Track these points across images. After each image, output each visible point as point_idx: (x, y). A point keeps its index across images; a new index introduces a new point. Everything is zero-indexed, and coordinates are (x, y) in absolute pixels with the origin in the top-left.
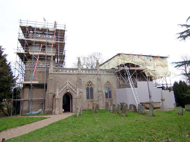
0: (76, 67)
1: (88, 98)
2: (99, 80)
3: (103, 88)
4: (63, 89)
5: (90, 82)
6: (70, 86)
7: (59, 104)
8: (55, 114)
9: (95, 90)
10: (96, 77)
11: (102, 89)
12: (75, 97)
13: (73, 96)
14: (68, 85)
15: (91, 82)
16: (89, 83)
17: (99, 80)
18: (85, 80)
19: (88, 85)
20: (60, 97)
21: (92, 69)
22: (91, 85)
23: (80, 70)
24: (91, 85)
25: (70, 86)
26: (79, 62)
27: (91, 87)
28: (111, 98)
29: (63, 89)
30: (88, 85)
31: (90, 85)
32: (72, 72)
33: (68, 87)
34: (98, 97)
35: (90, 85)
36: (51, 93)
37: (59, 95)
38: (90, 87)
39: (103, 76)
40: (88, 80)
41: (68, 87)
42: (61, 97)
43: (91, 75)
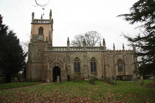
0: (66, 46)
1: (92, 71)
2: (85, 56)
3: (88, 63)
4: (53, 63)
5: (77, 58)
6: (58, 61)
7: (50, 76)
8: (26, 81)
9: (82, 65)
10: (83, 54)
11: (87, 64)
12: (62, 70)
13: (60, 69)
14: (57, 60)
15: (78, 58)
16: (93, 59)
17: (85, 56)
18: (73, 56)
19: (92, 60)
20: (51, 70)
21: (80, 47)
22: (94, 60)
23: (68, 48)
24: (94, 60)
25: (58, 61)
26: (68, 42)
27: (95, 62)
28: (79, 72)
29: (53, 63)
30: (92, 60)
31: (77, 60)
32: (76, 50)
33: (57, 62)
34: (84, 70)
35: (77, 60)
36: (46, 66)
37: (50, 69)
38: (93, 62)
39: (89, 53)
40: (76, 57)
41: (57, 62)
42: (51, 70)
43: (78, 52)
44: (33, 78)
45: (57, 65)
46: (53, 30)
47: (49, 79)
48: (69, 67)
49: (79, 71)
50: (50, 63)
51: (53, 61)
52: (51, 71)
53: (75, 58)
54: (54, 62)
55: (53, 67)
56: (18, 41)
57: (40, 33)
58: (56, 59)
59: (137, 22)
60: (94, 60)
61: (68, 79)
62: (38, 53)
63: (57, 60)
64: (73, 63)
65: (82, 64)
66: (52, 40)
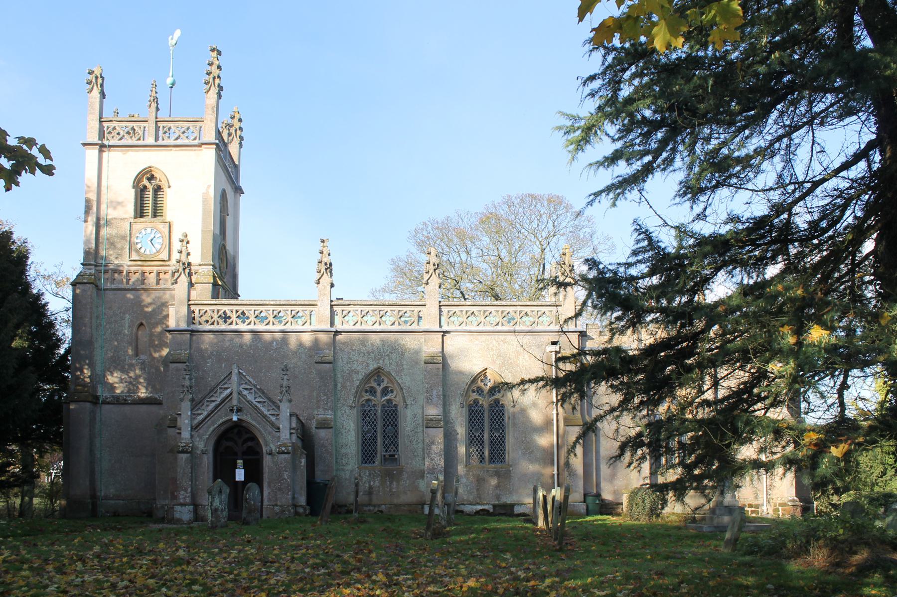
4: (213, 404)
6: (245, 392)
9: (408, 420)
24: (385, 391)
25: (245, 392)
27: (389, 401)
30: (372, 391)
40: (373, 366)
41: (235, 395)
42: (204, 443)
44: (107, 498)
45: (235, 418)
46: (238, 190)
47: (188, 500)
48: (322, 433)
49: (392, 459)
50: (196, 405)
51: (213, 390)
52: (203, 453)
53: (368, 377)
54: (224, 395)
55: (210, 430)
56: (20, 260)
57: (140, 213)
58: (234, 377)
59: (653, 174)
60: (386, 388)
61: (308, 503)
62: (137, 339)
63: (234, 384)
64: (351, 407)
65: (409, 413)
66: (235, 258)
